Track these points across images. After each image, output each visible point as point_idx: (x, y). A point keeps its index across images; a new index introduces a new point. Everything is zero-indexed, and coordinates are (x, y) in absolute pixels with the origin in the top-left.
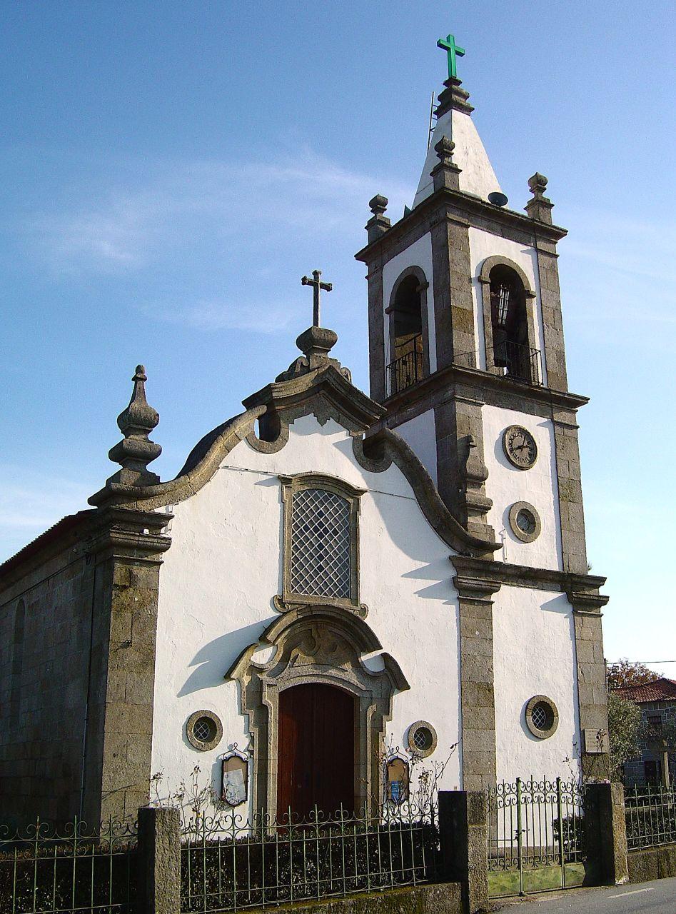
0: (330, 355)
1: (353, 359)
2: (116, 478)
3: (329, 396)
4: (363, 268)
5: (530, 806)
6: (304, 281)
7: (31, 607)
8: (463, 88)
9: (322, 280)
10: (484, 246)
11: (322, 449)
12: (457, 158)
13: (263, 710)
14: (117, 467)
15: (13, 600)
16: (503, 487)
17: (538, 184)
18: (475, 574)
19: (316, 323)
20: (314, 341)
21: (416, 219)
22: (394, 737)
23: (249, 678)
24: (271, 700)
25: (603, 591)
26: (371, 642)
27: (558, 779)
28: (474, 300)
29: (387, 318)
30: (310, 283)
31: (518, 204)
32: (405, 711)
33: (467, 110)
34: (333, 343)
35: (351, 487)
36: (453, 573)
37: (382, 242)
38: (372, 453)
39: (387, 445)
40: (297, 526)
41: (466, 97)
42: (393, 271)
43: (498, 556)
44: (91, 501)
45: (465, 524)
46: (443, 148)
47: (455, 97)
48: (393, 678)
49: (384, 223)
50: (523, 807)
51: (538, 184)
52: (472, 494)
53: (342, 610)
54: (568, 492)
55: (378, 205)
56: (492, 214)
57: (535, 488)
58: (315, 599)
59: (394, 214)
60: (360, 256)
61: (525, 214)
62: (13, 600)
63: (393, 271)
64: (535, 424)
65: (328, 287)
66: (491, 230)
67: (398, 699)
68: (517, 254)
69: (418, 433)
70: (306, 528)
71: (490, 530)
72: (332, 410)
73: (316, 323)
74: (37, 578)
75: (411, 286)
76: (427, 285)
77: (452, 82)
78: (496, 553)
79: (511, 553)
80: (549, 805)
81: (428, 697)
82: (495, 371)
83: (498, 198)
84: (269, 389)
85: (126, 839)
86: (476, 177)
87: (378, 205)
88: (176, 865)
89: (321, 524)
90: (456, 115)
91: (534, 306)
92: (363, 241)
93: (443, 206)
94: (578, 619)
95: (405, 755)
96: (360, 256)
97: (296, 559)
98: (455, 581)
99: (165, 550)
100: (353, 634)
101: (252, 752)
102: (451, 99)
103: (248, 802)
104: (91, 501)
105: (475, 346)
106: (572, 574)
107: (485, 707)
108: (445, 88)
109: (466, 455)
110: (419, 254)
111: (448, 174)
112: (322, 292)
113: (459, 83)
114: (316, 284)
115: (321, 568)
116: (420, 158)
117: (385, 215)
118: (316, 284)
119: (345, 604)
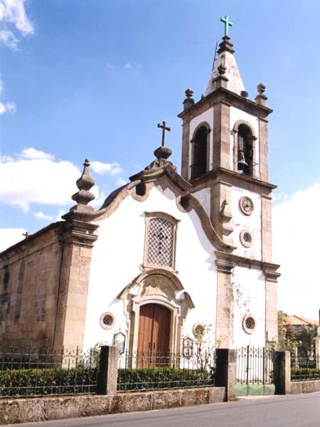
0: (168, 160)
1: (176, 160)
2: (75, 207)
3: (168, 179)
4: (181, 121)
5: (241, 358)
6: (159, 126)
7: (29, 263)
8: (230, 41)
9: (166, 126)
10: (236, 116)
11: (161, 199)
12: (226, 75)
13: (132, 313)
14: (75, 203)
15: (19, 259)
16: (238, 223)
17: (261, 88)
18: (227, 261)
19: (163, 145)
20: (162, 154)
21: (207, 101)
22: (187, 330)
23: (128, 301)
24: (136, 309)
25: (278, 271)
26: (179, 286)
27: (248, 347)
28: (231, 141)
29: (191, 145)
30: (161, 127)
31: (252, 97)
32: (192, 319)
33: (232, 52)
34: (170, 154)
35: (68, 214)
36: (215, 258)
37: (191, 109)
38: (186, 203)
39: (190, 201)
40: (151, 234)
41: (231, 45)
42: (195, 123)
43: (234, 253)
44: (63, 217)
45: (222, 238)
46: (222, 69)
47: (227, 46)
48: (187, 302)
49: (192, 101)
50: (250, 358)
51: (261, 88)
52: (226, 226)
53: (169, 272)
54: (264, 226)
55: (189, 93)
56: (239, 101)
57: (251, 223)
58: (158, 266)
59: (196, 98)
60: (180, 116)
61: (254, 101)
62: (19, 259)
63: (195, 123)
64: (255, 197)
65: (169, 129)
66: (239, 108)
67: (191, 313)
68: (252, 121)
69: (202, 196)
70: (155, 235)
71: (232, 241)
72: (169, 184)
73: (163, 145)
74: (35, 249)
75: (202, 131)
76: (210, 130)
77: (226, 38)
78: (234, 251)
79: (239, 252)
80: (244, 358)
81: (204, 312)
82: (237, 171)
83: (244, 94)
84: (142, 172)
85: (90, 363)
86: (235, 85)
87: (189, 93)
88: (116, 376)
89: (161, 234)
90: (227, 53)
91: (256, 144)
92: (181, 109)
93: (220, 96)
94: (267, 282)
95: (192, 337)
96: (180, 116)
97: (150, 248)
98: (216, 261)
99: (95, 240)
100: (170, 282)
101: (127, 331)
102: (224, 47)
103: (125, 353)
104: (63, 217)
105: (229, 161)
106: (265, 263)
107: (228, 317)
108: (222, 41)
109: (223, 208)
110: (207, 117)
111: (223, 82)
112: (166, 131)
113: (228, 39)
114: (163, 127)
115: (160, 253)
116: (210, 74)
117: (191, 98)
118: (163, 127)
119: (170, 269)
